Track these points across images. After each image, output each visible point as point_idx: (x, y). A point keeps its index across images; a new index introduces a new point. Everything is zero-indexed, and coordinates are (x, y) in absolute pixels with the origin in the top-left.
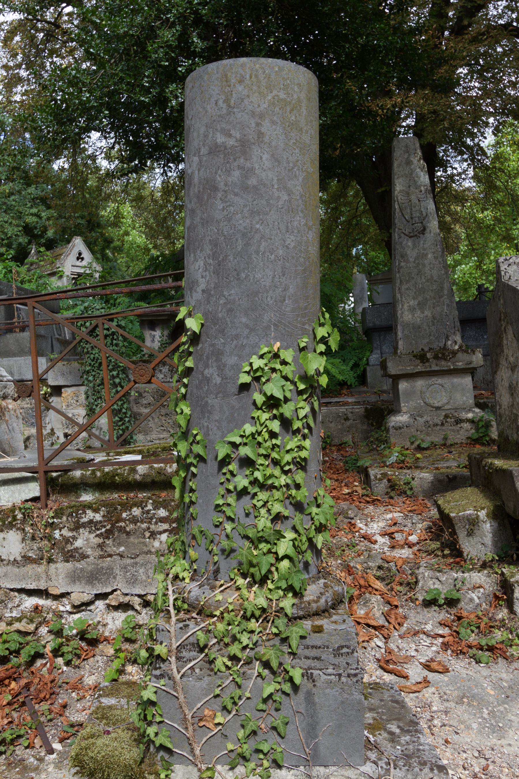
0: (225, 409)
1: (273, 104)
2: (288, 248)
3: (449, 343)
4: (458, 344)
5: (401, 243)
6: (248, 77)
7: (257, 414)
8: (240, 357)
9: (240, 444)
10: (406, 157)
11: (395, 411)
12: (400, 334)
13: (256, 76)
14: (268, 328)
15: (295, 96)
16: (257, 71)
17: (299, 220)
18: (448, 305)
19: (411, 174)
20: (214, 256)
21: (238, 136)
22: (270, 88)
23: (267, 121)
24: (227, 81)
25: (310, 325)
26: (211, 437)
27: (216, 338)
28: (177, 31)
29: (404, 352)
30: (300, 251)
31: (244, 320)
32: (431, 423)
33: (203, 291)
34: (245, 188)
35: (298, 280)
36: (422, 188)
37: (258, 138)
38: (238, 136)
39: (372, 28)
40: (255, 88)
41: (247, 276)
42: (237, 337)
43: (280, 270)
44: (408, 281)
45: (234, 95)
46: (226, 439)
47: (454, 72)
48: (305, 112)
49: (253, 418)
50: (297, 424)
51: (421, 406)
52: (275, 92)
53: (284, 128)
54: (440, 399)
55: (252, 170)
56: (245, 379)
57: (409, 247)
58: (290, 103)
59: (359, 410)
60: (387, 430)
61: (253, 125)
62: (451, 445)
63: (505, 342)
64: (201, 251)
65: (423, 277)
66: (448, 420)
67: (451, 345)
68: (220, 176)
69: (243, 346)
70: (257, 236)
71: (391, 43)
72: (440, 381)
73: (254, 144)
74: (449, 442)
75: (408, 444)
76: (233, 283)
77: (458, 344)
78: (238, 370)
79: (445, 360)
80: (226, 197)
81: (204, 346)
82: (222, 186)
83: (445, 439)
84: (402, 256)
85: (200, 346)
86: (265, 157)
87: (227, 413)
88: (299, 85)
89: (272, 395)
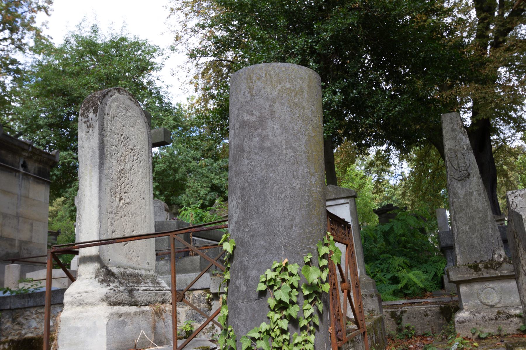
0: (249, 311)
1: (282, 92)
2: (294, 189)
3: (496, 256)
4: (503, 256)
5: (453, 185)
6: (264, 75)
7: (271, 314)
8: (259, 271)
9: (259, 339)
10: (451, 126)
11: (458, 308)
12: (457, 251)
13: (270, 75)
14: (280, 248)
15: (298, 86)
16: (270, 71)
17: (303, 169)
18: (492, 228)
19: (456, 138)
20: (242, 197)
21: (258, 114)
22: (279, 82)
23: (277, 103)
24: (250, 79)
25: (314, 245)
26: (240, 333)
27: (243, 257)
28: (299, 59)
29: (462, 264)
30: (305, 191)
31: (262, 243)
32: (487, 318)
33: (236, 222)
34: (262, 149)
35: (303, 212)
36: (465, 147)
37: (271, 114)
38: (258, 114)
39: (428, 47)
40: (268, 82)
41: (264, 210)
42: (257, 255)
43: (288, 206)
44: (460, 212)
45: (255, 88)
46: (248, 335)
47: (496, 70)
48: (306, 96)
49: (268, 318)
50: (303, 323)
51: (479, 305)
52: (283, 84)
53: (290, 107)
54: (493, 299)
55: (267, 136)
56: (262, 287)
57: (459, 187)
58: (294, 90)
59: (436, 308)
60: (454, 323)
61: (268, 106)
62: (505, 335)
63: (520, 254)
64: (235, 194)
65: (471, 209)
66: (501, 315)
67: (497, 258)
68: (246, 142)
69: (261, 263)
70: (271, 182)
71: (442, 55)
72: (491, 285)
73: (268, 119)
74: (503, 333)
75: (470, 335)
76: (254, 216)
77: (503, 256)
78: (257, 280)
79: (494, 269)
80: (250, 156)
81: (236, 263)
82: (247, 148)
83: (500, 330)
84: (454, 194)
85: (234, 263)
86: (276, 128)
87: (250, 314)
88: (301, 78)
89: (280, 299)
